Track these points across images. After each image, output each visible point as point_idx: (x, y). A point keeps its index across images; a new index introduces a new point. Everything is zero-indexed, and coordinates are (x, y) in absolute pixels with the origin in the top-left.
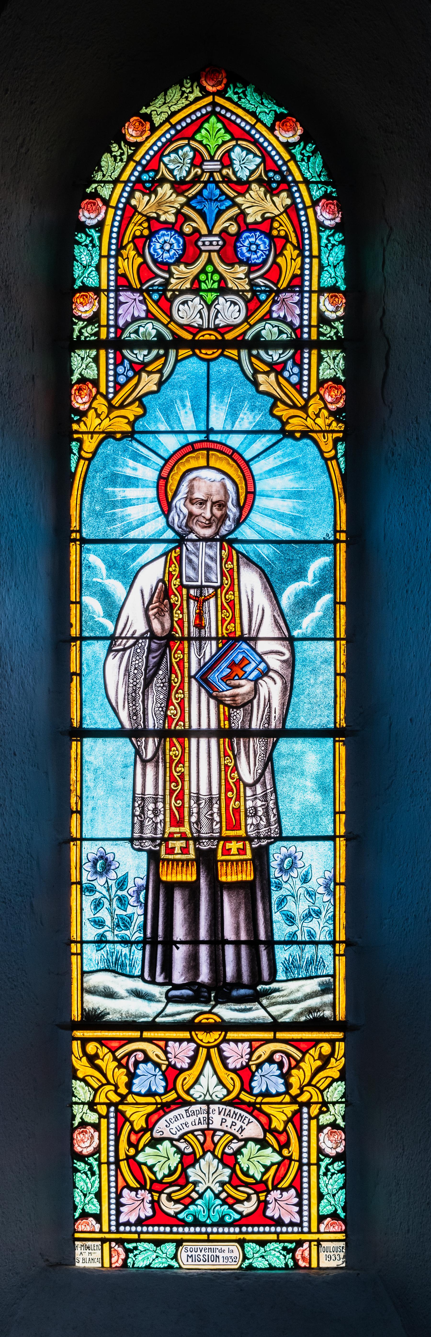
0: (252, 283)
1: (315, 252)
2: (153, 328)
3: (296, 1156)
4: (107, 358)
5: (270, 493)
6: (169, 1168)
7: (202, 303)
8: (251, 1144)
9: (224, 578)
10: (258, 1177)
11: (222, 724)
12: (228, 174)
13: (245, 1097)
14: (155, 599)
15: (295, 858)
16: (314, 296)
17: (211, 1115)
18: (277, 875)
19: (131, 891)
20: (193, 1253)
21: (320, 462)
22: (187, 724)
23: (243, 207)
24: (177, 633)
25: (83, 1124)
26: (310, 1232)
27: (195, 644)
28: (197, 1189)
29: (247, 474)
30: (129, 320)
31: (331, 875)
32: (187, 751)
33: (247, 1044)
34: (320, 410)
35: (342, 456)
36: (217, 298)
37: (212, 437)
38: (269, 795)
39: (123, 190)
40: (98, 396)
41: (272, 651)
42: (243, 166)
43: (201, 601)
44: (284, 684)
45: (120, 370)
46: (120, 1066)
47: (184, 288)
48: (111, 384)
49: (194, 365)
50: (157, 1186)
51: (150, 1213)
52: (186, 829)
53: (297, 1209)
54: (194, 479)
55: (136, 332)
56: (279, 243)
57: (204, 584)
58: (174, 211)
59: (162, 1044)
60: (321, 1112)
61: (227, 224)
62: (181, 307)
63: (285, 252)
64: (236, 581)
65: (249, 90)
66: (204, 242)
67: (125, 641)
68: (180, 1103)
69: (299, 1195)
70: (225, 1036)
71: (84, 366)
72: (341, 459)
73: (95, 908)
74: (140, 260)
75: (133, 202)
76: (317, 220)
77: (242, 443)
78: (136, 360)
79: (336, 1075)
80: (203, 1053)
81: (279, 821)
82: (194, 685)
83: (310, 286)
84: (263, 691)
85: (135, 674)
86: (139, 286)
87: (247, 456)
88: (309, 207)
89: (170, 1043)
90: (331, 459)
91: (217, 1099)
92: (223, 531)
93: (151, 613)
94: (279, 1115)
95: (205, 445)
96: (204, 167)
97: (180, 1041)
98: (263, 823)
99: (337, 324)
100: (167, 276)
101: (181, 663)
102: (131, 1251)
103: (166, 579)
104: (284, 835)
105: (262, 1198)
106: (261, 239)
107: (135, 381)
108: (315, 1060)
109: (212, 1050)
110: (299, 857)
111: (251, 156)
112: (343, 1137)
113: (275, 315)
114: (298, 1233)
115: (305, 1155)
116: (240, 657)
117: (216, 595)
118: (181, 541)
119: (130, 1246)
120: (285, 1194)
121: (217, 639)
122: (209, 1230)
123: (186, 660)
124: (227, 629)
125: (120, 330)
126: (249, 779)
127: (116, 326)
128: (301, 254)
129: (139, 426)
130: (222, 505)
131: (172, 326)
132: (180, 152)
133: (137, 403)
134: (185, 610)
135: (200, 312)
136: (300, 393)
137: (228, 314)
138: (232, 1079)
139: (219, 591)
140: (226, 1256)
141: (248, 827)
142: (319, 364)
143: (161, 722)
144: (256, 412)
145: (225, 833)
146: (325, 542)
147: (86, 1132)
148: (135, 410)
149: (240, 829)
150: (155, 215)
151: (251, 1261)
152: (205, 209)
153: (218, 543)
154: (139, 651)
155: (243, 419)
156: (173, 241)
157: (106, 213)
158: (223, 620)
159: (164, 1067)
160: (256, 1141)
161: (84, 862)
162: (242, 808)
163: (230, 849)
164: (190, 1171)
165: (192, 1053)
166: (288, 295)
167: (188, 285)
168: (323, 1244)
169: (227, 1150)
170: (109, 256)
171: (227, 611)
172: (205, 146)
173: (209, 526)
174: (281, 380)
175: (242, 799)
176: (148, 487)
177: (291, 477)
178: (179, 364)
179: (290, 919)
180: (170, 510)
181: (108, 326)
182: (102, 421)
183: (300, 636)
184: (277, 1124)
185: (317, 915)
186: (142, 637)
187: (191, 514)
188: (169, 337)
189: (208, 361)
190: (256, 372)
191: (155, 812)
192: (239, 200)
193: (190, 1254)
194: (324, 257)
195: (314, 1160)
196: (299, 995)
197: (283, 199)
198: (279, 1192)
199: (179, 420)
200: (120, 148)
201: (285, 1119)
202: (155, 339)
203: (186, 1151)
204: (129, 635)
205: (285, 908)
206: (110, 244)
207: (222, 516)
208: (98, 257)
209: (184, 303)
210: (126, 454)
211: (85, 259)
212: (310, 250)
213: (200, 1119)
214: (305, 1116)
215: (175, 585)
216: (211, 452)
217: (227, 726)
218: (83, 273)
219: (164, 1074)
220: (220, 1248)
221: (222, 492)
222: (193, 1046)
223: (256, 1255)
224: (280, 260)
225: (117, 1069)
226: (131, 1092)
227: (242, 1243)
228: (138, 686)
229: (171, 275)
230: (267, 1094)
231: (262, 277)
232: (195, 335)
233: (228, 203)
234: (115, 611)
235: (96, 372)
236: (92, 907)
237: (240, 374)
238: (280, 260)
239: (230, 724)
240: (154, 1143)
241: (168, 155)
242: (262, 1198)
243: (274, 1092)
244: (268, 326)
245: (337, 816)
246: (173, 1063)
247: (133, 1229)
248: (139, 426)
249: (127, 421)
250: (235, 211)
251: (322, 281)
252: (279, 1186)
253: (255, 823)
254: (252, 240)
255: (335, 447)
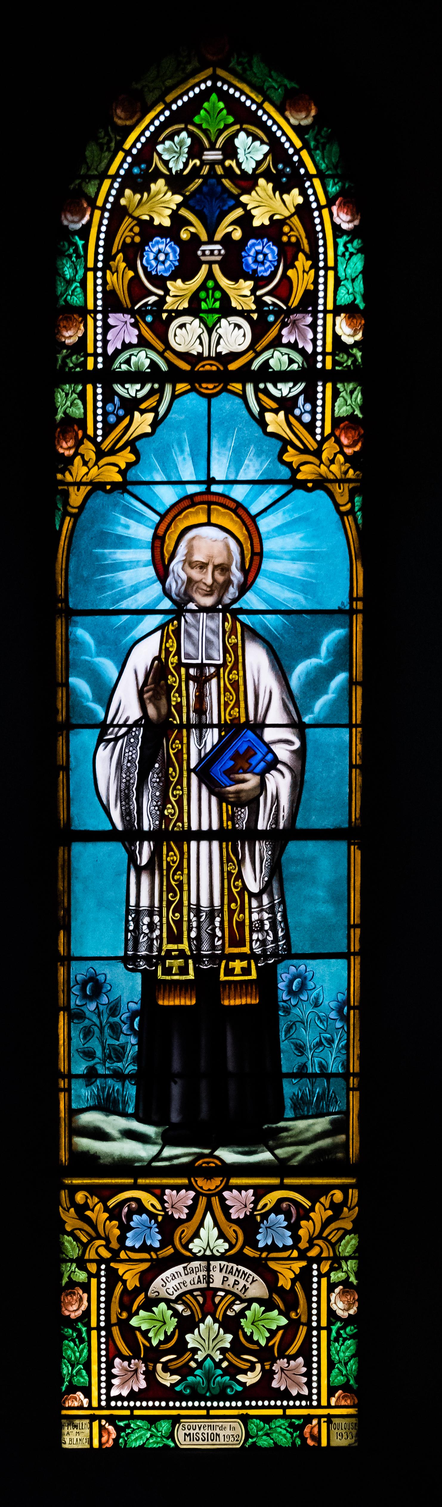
0: (258, 301)
1: (331, 263)
2: (147, 357)
3: (304, 1319)
4: (95, 394)
5: (278, 555)
6: (166, 1333)
7: (202, 326)
8: (255, 1306)
9: (228, 655)
10: (263, 1343)
11: (225, 825)
12: (231, 166)
13: (248, 1251)
14: (150, 680)
15: (305, 978)
16: (330, 317)
17: (211, 1273)
18: (285, 998)
19: (124, 1017)
20: (192, 1431)
21: (337, 517)
22: (186, 825)
23: (248, 208)
24: (175, 719)
25: (73, 1284)
26: (319, 1406)
27: (194, 732)
28: (196, 1357)
29: (252, 529)
30: (119, 347)
31: (345, 997)
32: (186, 856)
33: (251, 1191)
34: (335, 455)
35: (359, 510)
36: (219, 320)
37: (215, 488)
38: (277, 906)
39: (111, 187)
40: (85, 441)
41: (281, 740)
42: (248, 156)
43: (202, 681)
44: (294, 778)
45: (110, 408)
46: (110, 1219)
47: (180, 308)
48: (100, 425)
49: (194, 402)
50: (152, 1355)
51: (143, 1385)
52: (185, 946)
53: (305, 1380)
54: (194, 538)
55: (128, 362)
56: (290, 252)
57: (205, 661)
58: (169, 212)
59: (158, 1192)
60: (332, 1269)
61: (230, 229)
62: (178, 330)
63: (296, 263)
64: (240, 658)
65: (255, 60)
66: (204, 251)
67: (116, 729)
68: (177, 1259)
69: (308, 1364)
70: (228, 1181)
71: (68, 403)
72: (359, 513)
73: (85, 1038)
74: (131, 274)
75: (123, 202)
76: (333, 224)
77: (247, 495)
78: (127, 396)
79: (349, 1226)
80: (203, 1201)
81: (287, 936)
82: (194, 779)
83: (325, 304)
84: (271, 787)
85: (128, 768)
86: (130, 306)
87: (254, 510)
88: (324, 207)
89: (167, 1191)
90: (347, 513)
91: (218, 1254)
92: (227, 600)
93: (146, 696)
94: (287, 1273)
95: (205, 498)
96: (204, 157)
97: (178, 1188)
98: (270, 938)
99: (355, 351)
100: (161, 293)
101: (179, 754)
102: (123, 1429)
103: (163, 656)
104: (293, 951)
105: (267, 1367)
106: (269, 247)
107: (126, 421)
108: (325, 1209)
109: (213, 1199)
110: (309, 977)
111: (258, 143)
112: (356, 1297)
113: (285, 341)
114: (306, 1407)
115: (314, 1318)
116: (245, 747)
117: (217, 674)
118: (179, 611)
119: (122, 1424)
120: (292, 1362)
121: (219, 726)
122: (209, 1404)
123: (185, 751)
124: (230, 715)
125: (109, 360)
126: (254, 888)
127: (104, 354)
128: (315, 266)
129: (131, 476)
130: (224, 568)
131: (168, 354)
132: (176, 139)
133: (129, 448)
134: (184, 693)
135: (199, 337)
136: (313, 434)
137: (231, 340)
138: (235, 1231)
139: (222, 670)
140: (226, 1434)
141: (254, 943)
142: (334, 400)
143: (157, 822)
144: (263, 457)
145: (229, 950)
146: (340, 611)
147: (74, 1294)
148: (127, 456)
149: (245, 946)
150: (147, 218)
151: (254, 1440)
152: (205, 210)
153: (221, 614)
154: (132, 740)
155: (248, 466)
156: (168, 250)
157: (92, 216)
158: (226, 704)
159: (160, 1218)
160: (260, 1301)
161: (72, 984)
162: (247, 922)
163: (234, 969)
164: (188, 1337)
165: (190, 1202)
166: (299, 316)
167: (186, 305)
168: (335, 1421)
169: (229, 1313)
170: (95, 269)
171: (231, 694)
172: (205, 132)
173: (209, 594)
174: (292, 419)
175: (247, 911)
176: (141, 548)
177: (301, 535)
178: (176, 401)
179: (300, 1049)
180: (167, 575)
181: (95, 355)
182: (90, 470)
183: (312, 722)
184: (285, 1282)
185: (329, 1044)
186: (136, 724)
187: (190, 580)
188: (164, 367)
189: (209, 397)
190: (263, 410)
191: (151, 926)
192: (244, 199)
193: (187, 1432)
194: (341, 269)
195: (324, 1323)
196: (309, 1135)
197: (295, 197)
198: (285, 1360)
199: (177, 468)
200: (107, 134)
201: (293, 1276)
202: (149, 370)
203: (184, 1314)
204: (121, 722)
205: (294, 1036)
206: (97, 254)
207: (225, 582)
208: (83, 271)
209: (182, 326)
210: (117, 509)
211: (68, 273)
212: (325, 260)
213: (199, 1277)
214: (315, 1273)
215: (172, 663)
216: (212, 507)
217: (230, 827)
218: (66, 290)
219: (160, 1225)
220: (220, 1424)
221: (225, 553)
222: (192, 1194)
223: (260, 1433)
224: (291, 273)
225: (108, 1222)
226: (124, 1247)
227: (245, 1419)
228: (132, 781)
229: (167, 292)
230: (273, 1248)
231: (268, 294)
232: (193, 366)
233: (232, 203)
234: (106, 694)
235: (82, 411)
236: (81, 1036)
237: (245, 412)
238: (291, 273)
239: (234, 825)
240: (149, 1304)
241: (163, 142)
242: (267, 1367)
243: (281, 1246)
244: (277, 354)
245: (352, 930)
246: (170, 1213)
247: (126, 1404)
248: (131, 476)
249: (117, 469)
250: (239, 212)
251: (338, 298)
252: (287, 1353)
253: (261, 938)
254: (259, 248)
255: (351, 500)
